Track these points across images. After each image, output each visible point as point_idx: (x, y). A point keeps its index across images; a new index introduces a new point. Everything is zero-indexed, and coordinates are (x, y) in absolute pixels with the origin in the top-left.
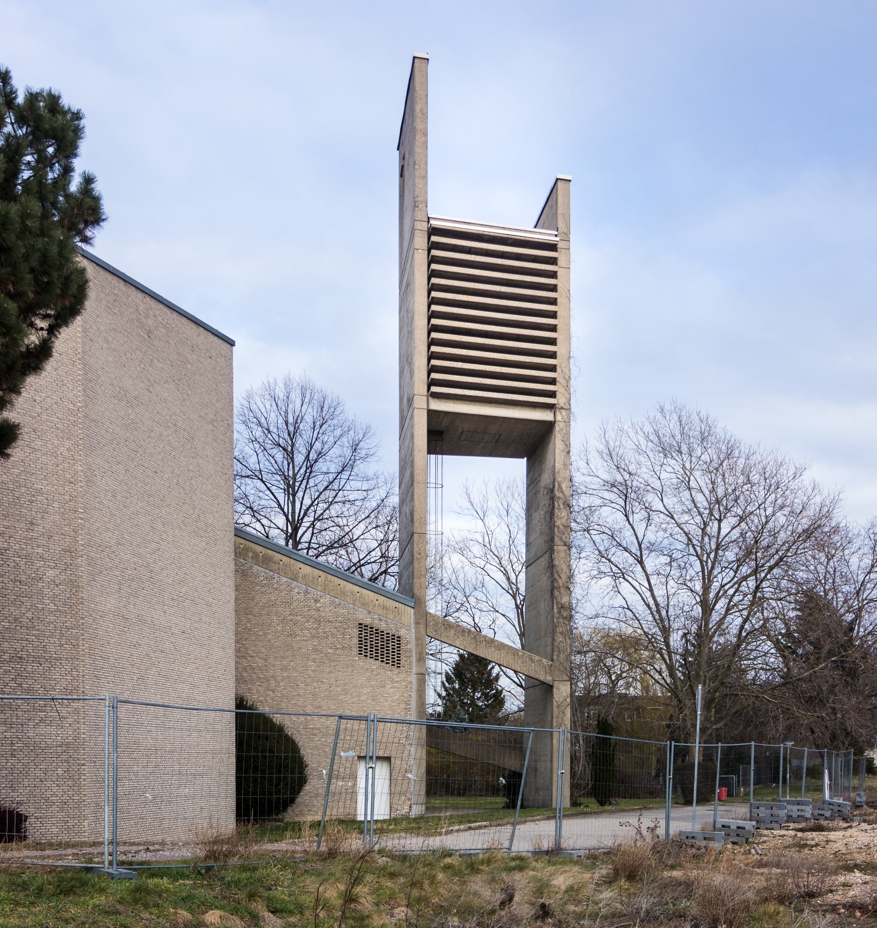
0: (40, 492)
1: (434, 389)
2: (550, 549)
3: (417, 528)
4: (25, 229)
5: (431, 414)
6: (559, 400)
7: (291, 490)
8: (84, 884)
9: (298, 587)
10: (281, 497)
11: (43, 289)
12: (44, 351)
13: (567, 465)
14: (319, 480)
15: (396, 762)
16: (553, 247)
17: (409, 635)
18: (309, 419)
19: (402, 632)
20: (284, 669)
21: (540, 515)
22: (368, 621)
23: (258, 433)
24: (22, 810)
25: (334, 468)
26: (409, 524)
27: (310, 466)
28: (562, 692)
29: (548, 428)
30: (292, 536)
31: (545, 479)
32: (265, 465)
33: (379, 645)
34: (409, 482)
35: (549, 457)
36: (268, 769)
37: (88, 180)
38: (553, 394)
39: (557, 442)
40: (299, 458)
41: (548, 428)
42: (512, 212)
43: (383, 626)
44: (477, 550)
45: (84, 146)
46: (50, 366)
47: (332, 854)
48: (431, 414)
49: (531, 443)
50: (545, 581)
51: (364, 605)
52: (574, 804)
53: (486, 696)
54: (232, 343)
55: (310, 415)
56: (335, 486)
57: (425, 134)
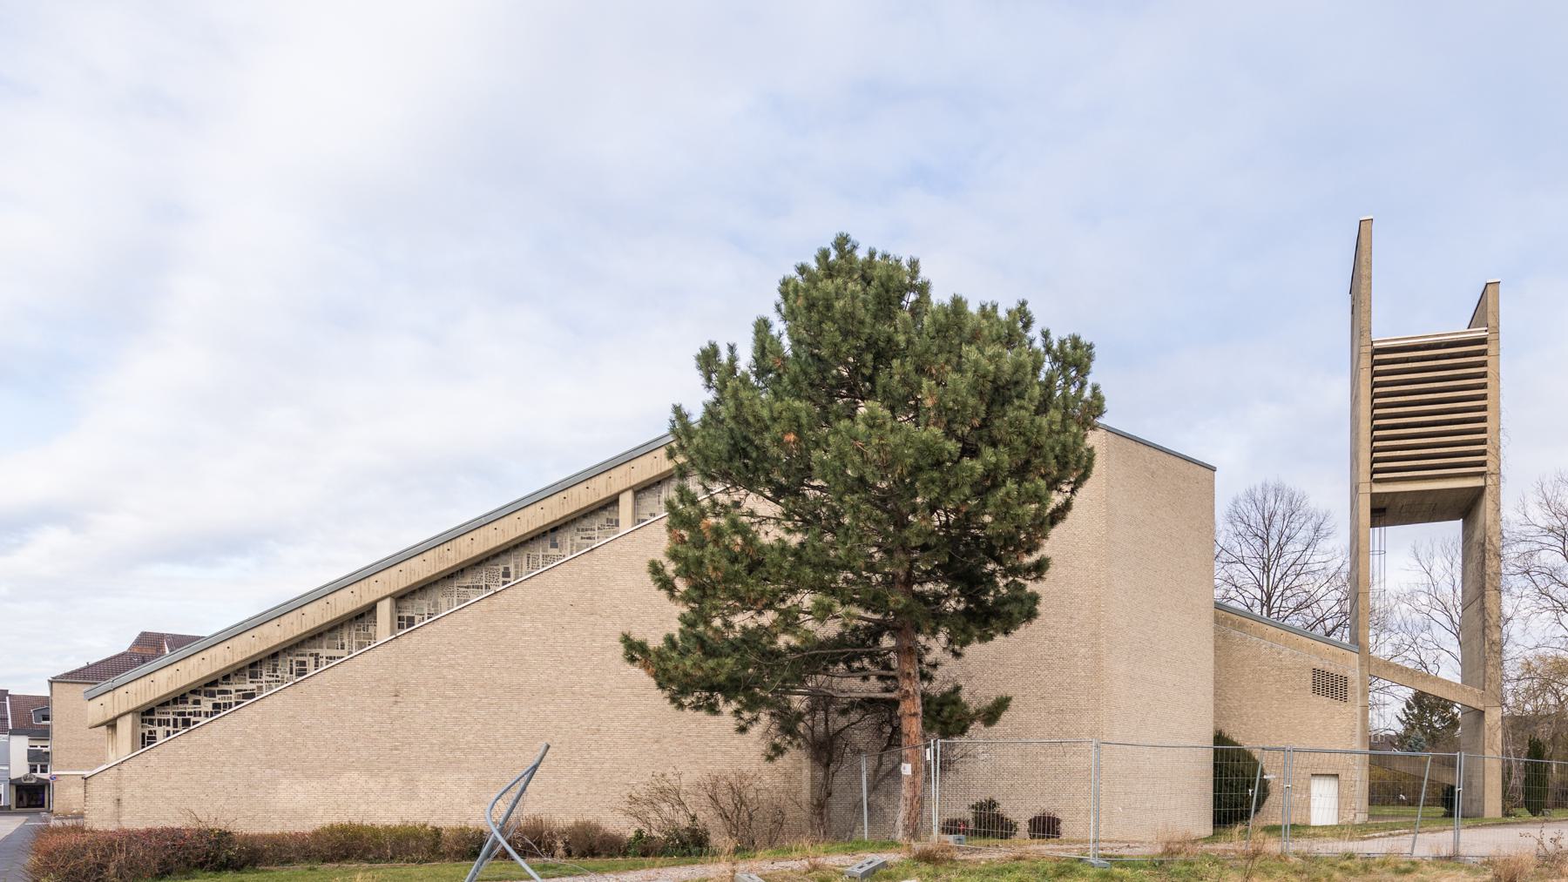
0: (1077, 596)
1: (1376, 476)
2: (1482, 595)
3: (1362, 588)
4: (1051, 431)
5: (1374, 496)
6: (1490, 467)
7: (1266, 569)
8: (1072, 870)
9: (1265, 644)
10: (1257, 572)
11: (1063, 464)
12: (1067, 506)
13: (1497, 521)
14: (1288, 558)
15: (1343, 777)
16: (1483, 341)
17: (1354, 674)
18: (1280, 512)
19: (1349, 674)
20: (1255, 707)
21: (1472, 566)
22: (1320, 666)
23: (1241, 528)
24: (1059, 816)
25: (1300, 547)
26: (1357, 585)
27: (1280, 547)
28: (1494, 716)
29: (1479, 492)
30: (1267, 602)
31: (1478, 535)
32: (1247, 552)
33: (1330, 685)
34: (1357, 551)
35: (1481, 516)
36: (1236, 787)
37: (1095, 388)
38: (1483, 464)
39: (1488, 502)
40: (1272, 544)
41: (1479, 492)
42: (1449, 320)
43: (1332, 670)
44: (1424, 599)
45: (1094, 366)
46: (1070, 515)
47: (1256, 854)
48: (1374, 496)
49: (1466, 507)
50: (1477, 622)
51: (1318, 654)
52: (1506, 814)
53: (1443, 719)
54: (1214, 469)
55: (1281, 508)
56: (1301, 561)
57: (1370, 278)
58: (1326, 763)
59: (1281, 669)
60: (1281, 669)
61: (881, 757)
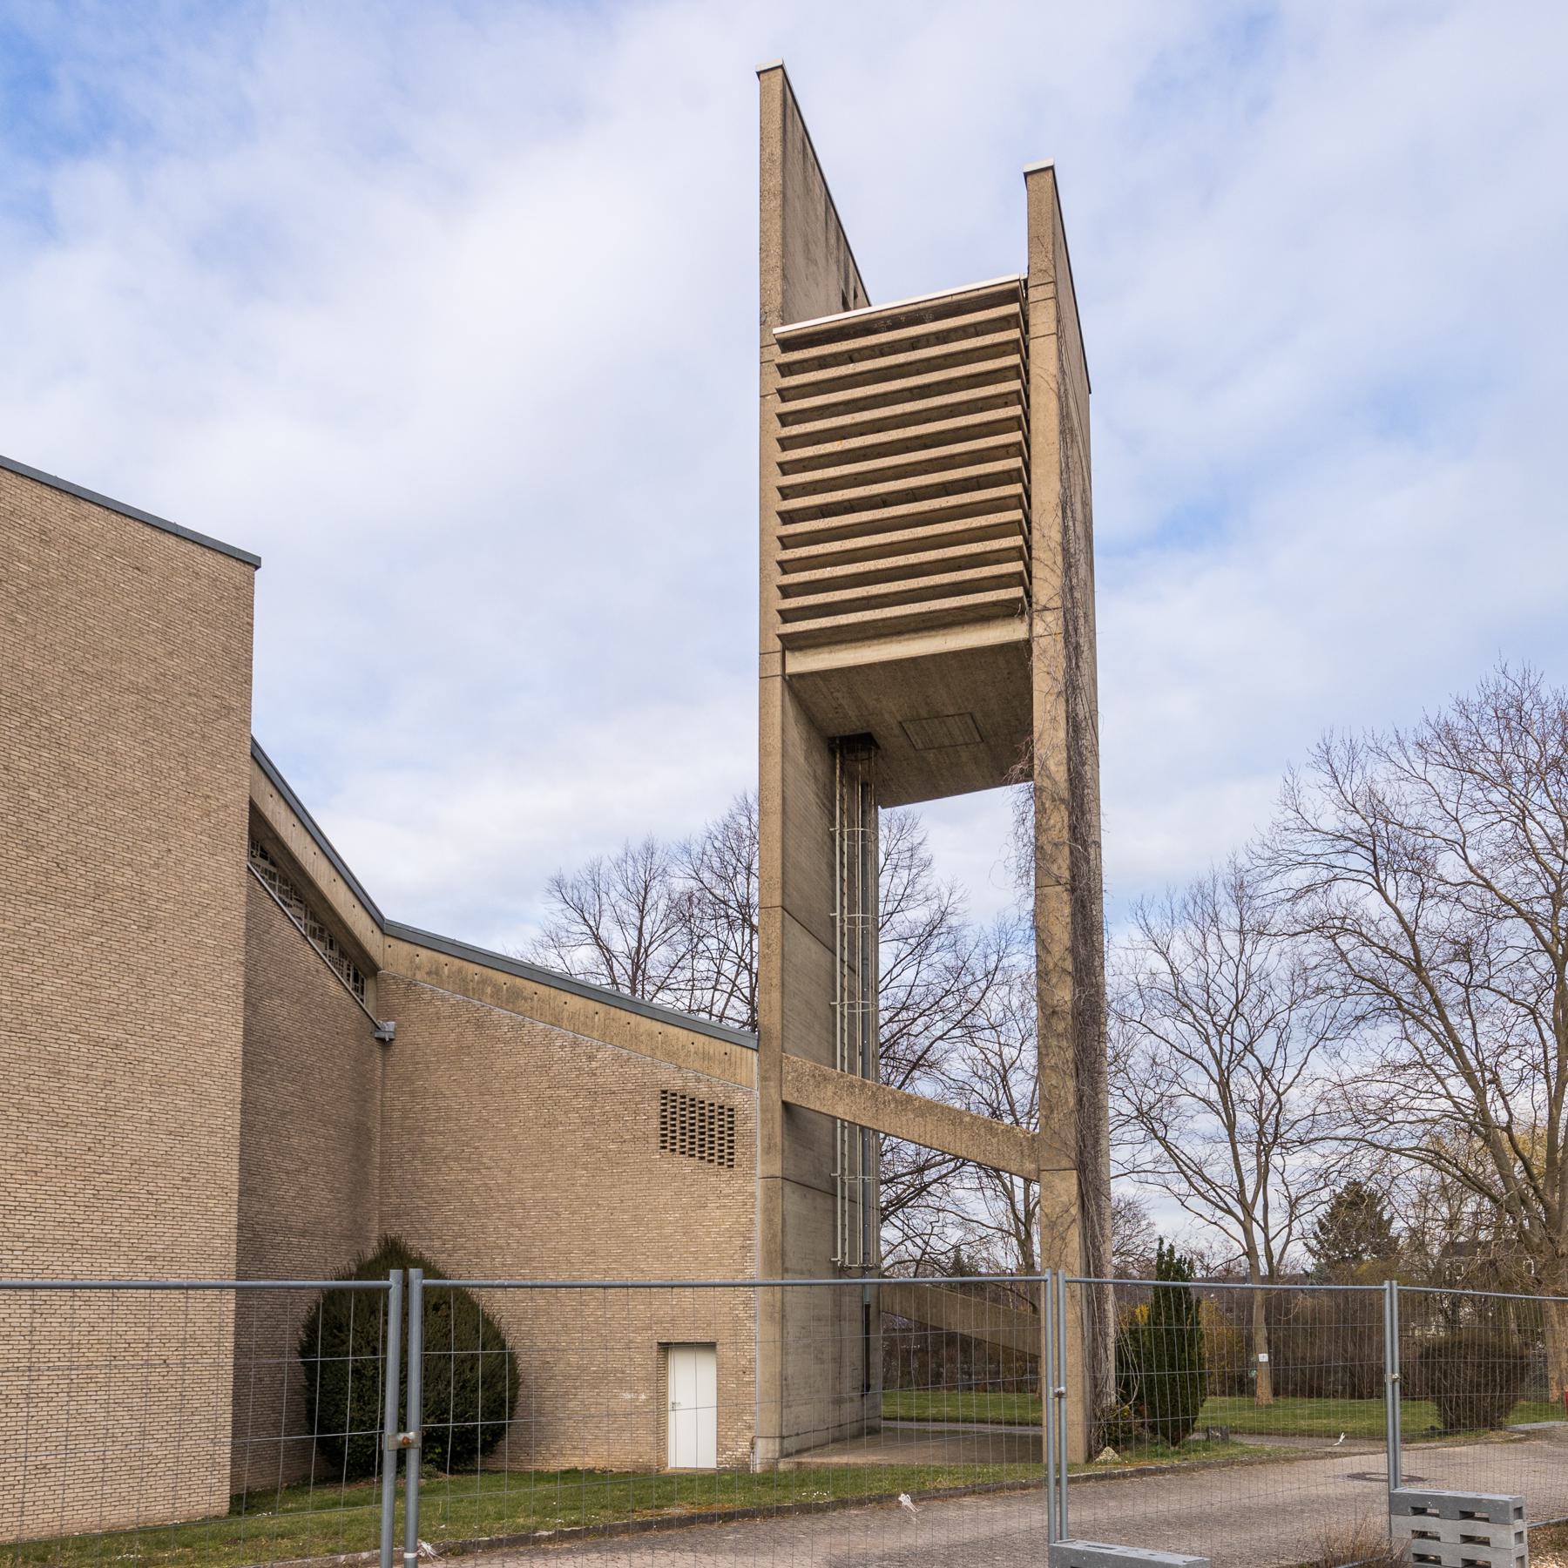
9: (562, 1036)
19: (738, 1100)
22: (676, 1084)
43: (702, 1092)
54: (253, 563)
58: (679, 1314)
59: (593, 1094)
60: (593, 1094)
61: (1511, 1115)
